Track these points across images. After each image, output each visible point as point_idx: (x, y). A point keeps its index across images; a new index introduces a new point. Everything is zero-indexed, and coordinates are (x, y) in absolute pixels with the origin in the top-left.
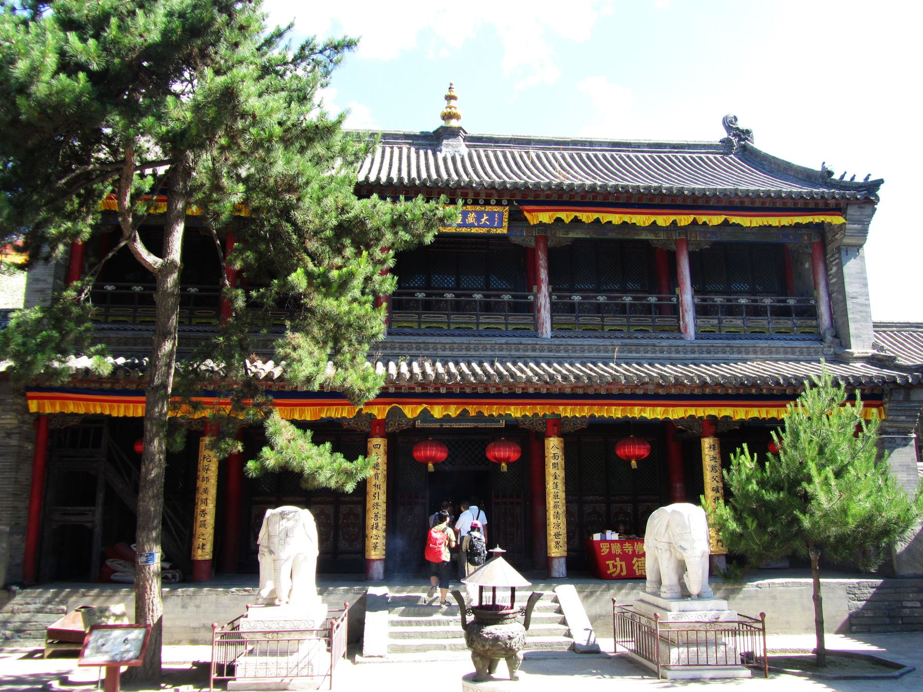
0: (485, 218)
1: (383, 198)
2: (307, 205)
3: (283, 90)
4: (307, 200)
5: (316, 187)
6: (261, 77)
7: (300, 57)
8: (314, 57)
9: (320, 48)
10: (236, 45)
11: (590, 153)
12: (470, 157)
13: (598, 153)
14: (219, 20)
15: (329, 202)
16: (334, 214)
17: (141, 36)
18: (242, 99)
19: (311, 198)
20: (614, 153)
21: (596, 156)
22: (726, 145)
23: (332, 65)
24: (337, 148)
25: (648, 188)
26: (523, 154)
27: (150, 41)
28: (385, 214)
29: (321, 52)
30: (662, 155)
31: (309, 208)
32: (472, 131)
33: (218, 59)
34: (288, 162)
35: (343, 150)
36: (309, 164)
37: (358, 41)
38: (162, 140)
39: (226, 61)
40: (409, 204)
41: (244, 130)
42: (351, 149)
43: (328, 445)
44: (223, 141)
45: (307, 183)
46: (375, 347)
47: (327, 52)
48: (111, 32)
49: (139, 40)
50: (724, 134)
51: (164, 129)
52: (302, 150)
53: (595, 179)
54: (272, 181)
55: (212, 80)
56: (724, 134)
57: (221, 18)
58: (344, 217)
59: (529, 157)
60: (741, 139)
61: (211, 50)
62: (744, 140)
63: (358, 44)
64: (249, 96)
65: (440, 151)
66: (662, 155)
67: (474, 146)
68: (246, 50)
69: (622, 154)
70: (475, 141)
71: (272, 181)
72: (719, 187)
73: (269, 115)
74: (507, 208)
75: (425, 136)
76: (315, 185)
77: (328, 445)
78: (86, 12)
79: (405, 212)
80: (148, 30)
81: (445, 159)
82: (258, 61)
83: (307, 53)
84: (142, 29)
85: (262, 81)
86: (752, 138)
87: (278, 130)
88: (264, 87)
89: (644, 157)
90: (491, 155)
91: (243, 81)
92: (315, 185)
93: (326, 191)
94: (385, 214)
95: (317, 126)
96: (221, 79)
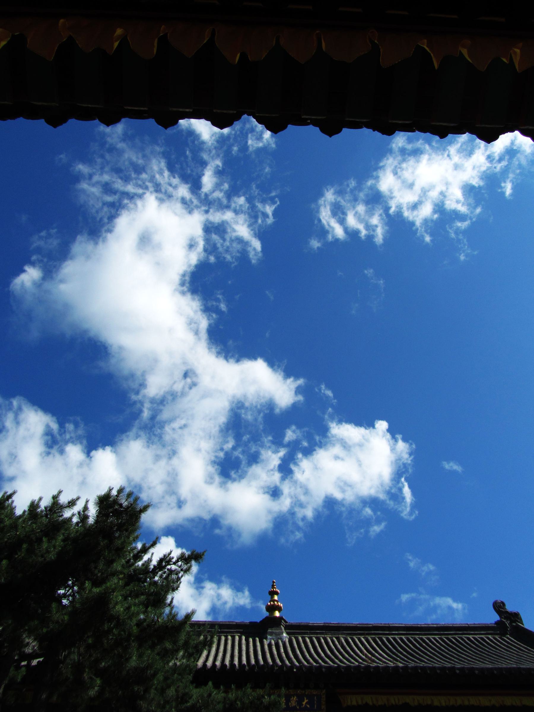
0: (306, 701)
1: (216, 686)
2: (152, 696)
3: (142, 594)
4: (153, 691)
5: (161, 678)
6: (127, 584)
7: (158, 568)
8: (169, 567)
9: (174, 560)
10: (112, 562)
11: (390, 637)
12: (290, 641)
13: (396, 637)
14: (102, 544)
15: (171, 692)
16: (174, 704)
17: (42, 556)
18: (111, 606)
19: (156, 689)
20: (409, 637)
21: (395, 639)
22: (498, 628)
23: (182, 573)
24: (181, 642)
25: (443, 669)
26: (334, 639)
27: (48, 559)
28: (219, 703)
29: (175, 563)
30: (450, 637)
31: (153, 699)
32: (292, 620)
33: (96, 571)
34: (140, 656)
35: (186, 644)
36: (158, 657)
37: (203, 554)
38: (40, 639)
39: (102, 574)
40: (240, 693)
41: (110, 631)
42: (192, 643)
43: (382, 425)
44: (90, 641)
45: (154, 675)
46: (32, 511)
47: (180, 563)
48: (21, 555)
49: (40, 559)
50: (497, 618)
51: (45, 630)
52: (152, 647)
53: (397, 660)
54: (124, 673)
55: (90, 591)
56: (497, 618)
57: (103, 543)
58: (183, 706)
59: (339, 642)
60: (512, 622)
61: (93, 565)
62: (515, 622)
63: (203, 557)
64: (117, 603)
65: (266, 638)
66: (450, 637)
67: (293, 634)
68: (117, 566)
69: (417, 637)
70: (295, 629)
71: (124, 673)
72: (504, 666)
73: (130, 618)
74: (324, 691)
75: (253, 625)
76: (160, 677)
77: (382, 425)
78: (6, 540)
79: (235, 701)
80: (48, 552)
81: (270, 645)
82: (126, 571)
83: (164, 564)
84: (44, 551)
85: (128, 588)
86: (521, 619)
87: (135, 630)
88: (128, 592)
89: (435, 639)
90: (308, 640)
91: (114, 592)
92: (160, 677)
93: (169, 682)
94: (219, 703)
95: (167, 626)
96: (96, 590)
